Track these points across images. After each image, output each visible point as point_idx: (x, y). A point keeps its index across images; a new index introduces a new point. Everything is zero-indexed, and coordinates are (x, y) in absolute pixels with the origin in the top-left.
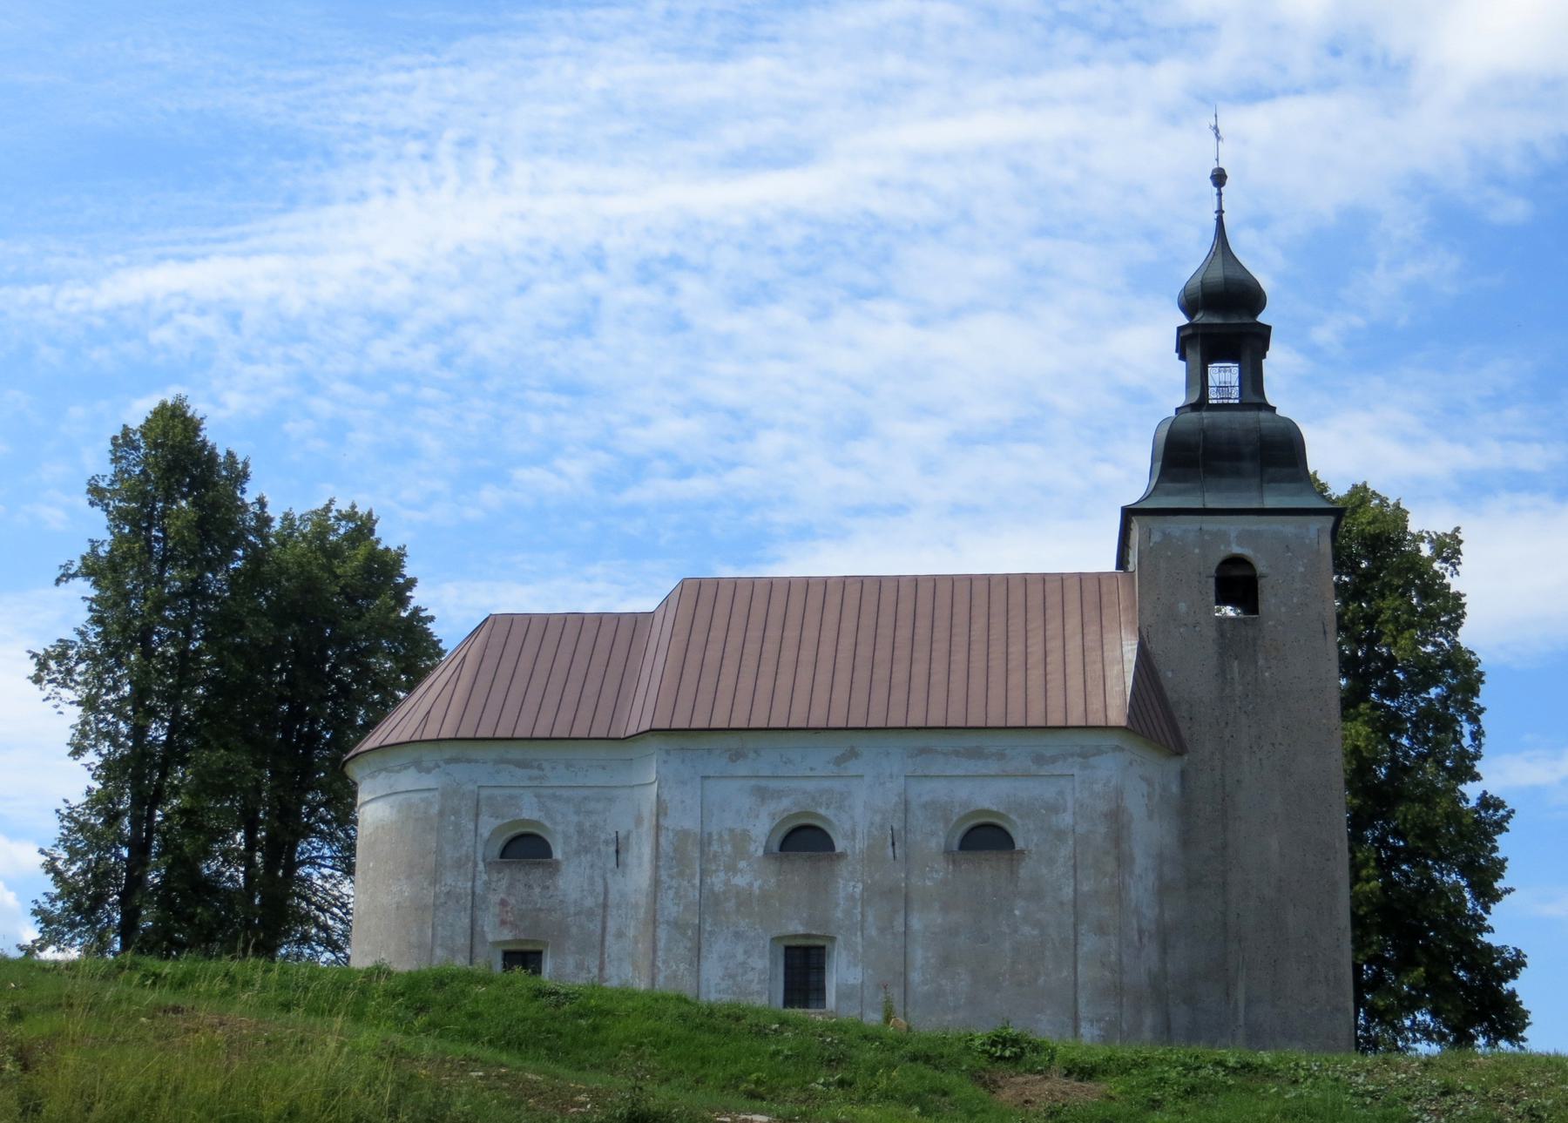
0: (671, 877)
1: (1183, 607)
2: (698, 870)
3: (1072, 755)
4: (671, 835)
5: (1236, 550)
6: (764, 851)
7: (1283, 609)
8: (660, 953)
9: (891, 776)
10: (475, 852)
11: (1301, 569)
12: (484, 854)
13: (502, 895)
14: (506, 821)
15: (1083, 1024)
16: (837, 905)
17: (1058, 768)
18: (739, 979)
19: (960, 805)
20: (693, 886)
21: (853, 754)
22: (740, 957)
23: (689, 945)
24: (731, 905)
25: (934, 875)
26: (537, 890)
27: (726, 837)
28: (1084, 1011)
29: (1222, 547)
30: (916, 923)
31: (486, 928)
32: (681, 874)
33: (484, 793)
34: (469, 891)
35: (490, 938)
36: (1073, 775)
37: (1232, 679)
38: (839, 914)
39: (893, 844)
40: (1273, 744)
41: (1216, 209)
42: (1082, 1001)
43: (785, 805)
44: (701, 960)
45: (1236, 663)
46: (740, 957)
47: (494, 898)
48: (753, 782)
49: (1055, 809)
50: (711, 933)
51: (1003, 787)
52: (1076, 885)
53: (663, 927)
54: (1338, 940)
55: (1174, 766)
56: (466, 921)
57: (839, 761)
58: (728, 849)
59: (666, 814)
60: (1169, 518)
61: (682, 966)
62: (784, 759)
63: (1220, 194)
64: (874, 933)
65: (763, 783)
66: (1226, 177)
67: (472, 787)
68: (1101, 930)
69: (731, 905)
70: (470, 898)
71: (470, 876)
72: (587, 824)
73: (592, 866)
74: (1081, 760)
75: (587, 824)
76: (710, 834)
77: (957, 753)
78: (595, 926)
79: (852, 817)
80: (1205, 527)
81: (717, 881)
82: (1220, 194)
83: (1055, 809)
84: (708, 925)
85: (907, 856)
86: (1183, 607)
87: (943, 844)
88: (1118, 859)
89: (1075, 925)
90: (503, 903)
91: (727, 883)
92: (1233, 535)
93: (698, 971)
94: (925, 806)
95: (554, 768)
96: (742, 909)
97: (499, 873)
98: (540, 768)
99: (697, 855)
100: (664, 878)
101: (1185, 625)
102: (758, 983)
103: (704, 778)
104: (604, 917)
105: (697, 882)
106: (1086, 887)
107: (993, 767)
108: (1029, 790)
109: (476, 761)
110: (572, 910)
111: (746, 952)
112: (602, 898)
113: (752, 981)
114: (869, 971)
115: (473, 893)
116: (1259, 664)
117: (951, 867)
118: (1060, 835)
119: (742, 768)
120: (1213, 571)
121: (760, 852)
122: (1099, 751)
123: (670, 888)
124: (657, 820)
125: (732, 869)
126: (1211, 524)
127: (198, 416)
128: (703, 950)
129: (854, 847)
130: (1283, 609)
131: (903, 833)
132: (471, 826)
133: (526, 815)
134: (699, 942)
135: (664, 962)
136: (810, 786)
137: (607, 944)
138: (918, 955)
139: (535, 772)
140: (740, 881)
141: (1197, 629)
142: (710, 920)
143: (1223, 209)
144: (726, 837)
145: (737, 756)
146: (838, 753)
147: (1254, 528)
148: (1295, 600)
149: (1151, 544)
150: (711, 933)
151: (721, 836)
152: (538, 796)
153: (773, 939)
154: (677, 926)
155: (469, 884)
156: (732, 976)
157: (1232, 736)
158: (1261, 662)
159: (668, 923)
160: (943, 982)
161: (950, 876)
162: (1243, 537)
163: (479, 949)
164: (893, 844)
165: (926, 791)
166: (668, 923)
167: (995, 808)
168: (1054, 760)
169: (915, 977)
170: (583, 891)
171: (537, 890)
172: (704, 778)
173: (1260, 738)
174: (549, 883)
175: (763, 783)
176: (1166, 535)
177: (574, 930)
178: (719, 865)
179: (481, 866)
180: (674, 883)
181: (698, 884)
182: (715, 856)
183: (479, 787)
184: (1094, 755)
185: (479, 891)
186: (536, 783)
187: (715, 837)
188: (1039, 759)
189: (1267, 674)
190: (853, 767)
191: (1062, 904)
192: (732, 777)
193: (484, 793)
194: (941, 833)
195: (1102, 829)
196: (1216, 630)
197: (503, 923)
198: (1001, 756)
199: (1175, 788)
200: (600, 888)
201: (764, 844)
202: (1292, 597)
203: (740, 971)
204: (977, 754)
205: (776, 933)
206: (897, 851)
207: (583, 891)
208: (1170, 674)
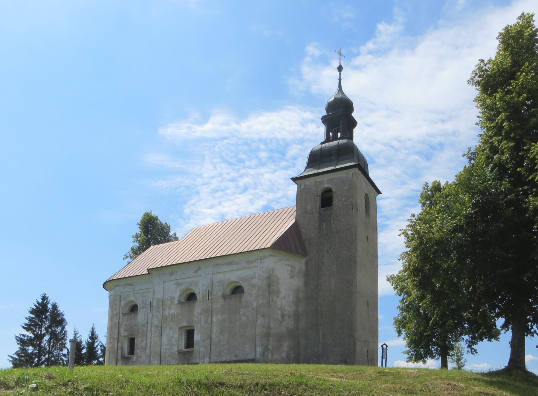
0: (156, 312)
1: (309, 208)
2: (162, 310)
3: (257, 260)
4: (156, 300)
5: (326, 186)
6: (178, 302)
7: (340, 203)
8: (152, 335)
9: (209, 274)
10: (120, 311)
11: (346, 188)
12: (122, 311)
13: (125, 323)
14: (127, 301)
15: (257, 347)
16: (195, 316)
17: (254, 264)
18: (171, 341)
19: (227, 280)
20: (161, 315)
21: (199, 269)
22: (171, 334)
23: (159, 332)
24: (169, 319)
25: (219, 304)
26: (133, 320)
27: (169, 299)
28: (258, 343)
29: (322, 186)
30: (214, 319)
31: (122, 332)
32: (158, 311)
33: (122, 294)
34: (118, 322)
35: (122, 335)
36: (257, 266)
37: (323, 229)
38: (195, 319)
39: (208, 295)
40: (334, 249)
41: (339, 78)
42: (257, 340)
43: (183, 287)
44: (162, 336)
45: (324, 224)
46: (171, 334)
47: (124, 324)
48: (176, 281)
49: (253, 278)
50: (165, 328)
51: (239, 273)
52: (257, 302)
53: (153, 327)
54: (352, 312)
55: (304, 260)
56: (117, 331)
57: (196, 272)
58: (169, 302)
59: (155, 294)
60: (306, 179)
61: (157, 338)
62: (183, 273)
63: (340, 74)
64: (203, 324)
65: (178, 281)
66: (342, 68)
67: (119, 293)
68: (263, 316)
69: (169, 319)
70: (118, 324)
71: (118, 318)
72: (144, 300)
73: (145, 312)
74: (260, 261)
75: (144, 300)
76: (165, 299)
77: (226, 264)
78: (145, 329)
79: (199, 288)
80: (317, 180)
81: (166, 312)
82: (340, 74)
83: (253, 278)
84: (164, 326)
85: (212, 298)
86: (309, 208)
87: (222, 293)
88: (269, 292)
89: (257, 315)
90: (126, 325)
91: (169, 313)
92: (326, 181)
93: (161, 340)
94: (218, 282)
95: (137, 285)
96: (172, 320)
97: (125, 316)
98: (134, 286)
99: (161, 305)
100: (154, 313)
101: (309, 214)
102: (176, 342)
103: (164, 282)
104: (147, 326)
105: (161, 313)
106: (260, 302)
107: (235, 267)
108: (246, 273)
109: (120, 286)
110: (140, 325)
111: (173, 333)
112: (147, 321)
113: (174, 341)
114: (202, 336)
115: (119, 323)
116: (331, 222)
117: (224, 300)
118: (254, 286)
119: (173, 278)
120: (320, 194)
121: (177, 302)
122: (265, 257)
123: (155, 316)
124: (153, 297)
125: (170, 308)
126: (318, 178)
127: (156, 215)
128: (163, 333)
129: (199, 298)
130: (340, 203)
131: (211, 291)
132: (119, 304)
133: (131, 299)
134: (162, 331)
135: (154, 338)
136: (189, 280)
137: (148, 334)
138: (215, 329)
139: (133, 287)
140: (172, 312)
141: (313, 214)
142: (164, 324)
143: (341, 78)
144: (169, 299)
145: (172, 274)
146: (196, 269)
147: (332, 177)
148: (344, 199)
149: (301, 189)
150: (165, 328)
151: (168, 299)
152: (134, 293)
153: (180, 328)
154: (157, 327)
155: (118, 320)
156: (169, 340)
157: (322, 248)
158: (332, 222)
159: (154, 326)
160: (221, 337)
161: (224, 304)
162: (331, 181)
163: (120, 339)
164: (208, 295)
165: (218, 278)
166: (154, 326)
167: (236, 280)
168: (252, 262)
169: (214, 336)
170: (143, 319)
171: (133, 320)
172: (164, 282)
173: (330, 247)
174: (135, 318)
175: (178, 281)
176: (305, 186)
177: (141, 331)
178: (167, 307)
179: (121, 314)
180: (156, 314)
181: (161, 314)
182: (166, 305)
183: (121, 293)
184: (264, 259)
185: (120, 322)
186: (133, 290)
187: (167, 299)
188: (248, 262)
189: (334, 225)
190: (199, 273)
191: (253, 309)
192: (171, 280)
193: (122, 294)
194: (221, 290)
195: (265, 283)
196: (319, 213)
197: (125, 330)
198: (238, 263)
199: (304, 268)
200: (146, 318)
201: (178, 299)
202: (343, 198)
203: (171, 338)
204: (231, 263)
205: (180, 326)
206: (209, 297)
207: (143, 319)
208: (304, 231)
